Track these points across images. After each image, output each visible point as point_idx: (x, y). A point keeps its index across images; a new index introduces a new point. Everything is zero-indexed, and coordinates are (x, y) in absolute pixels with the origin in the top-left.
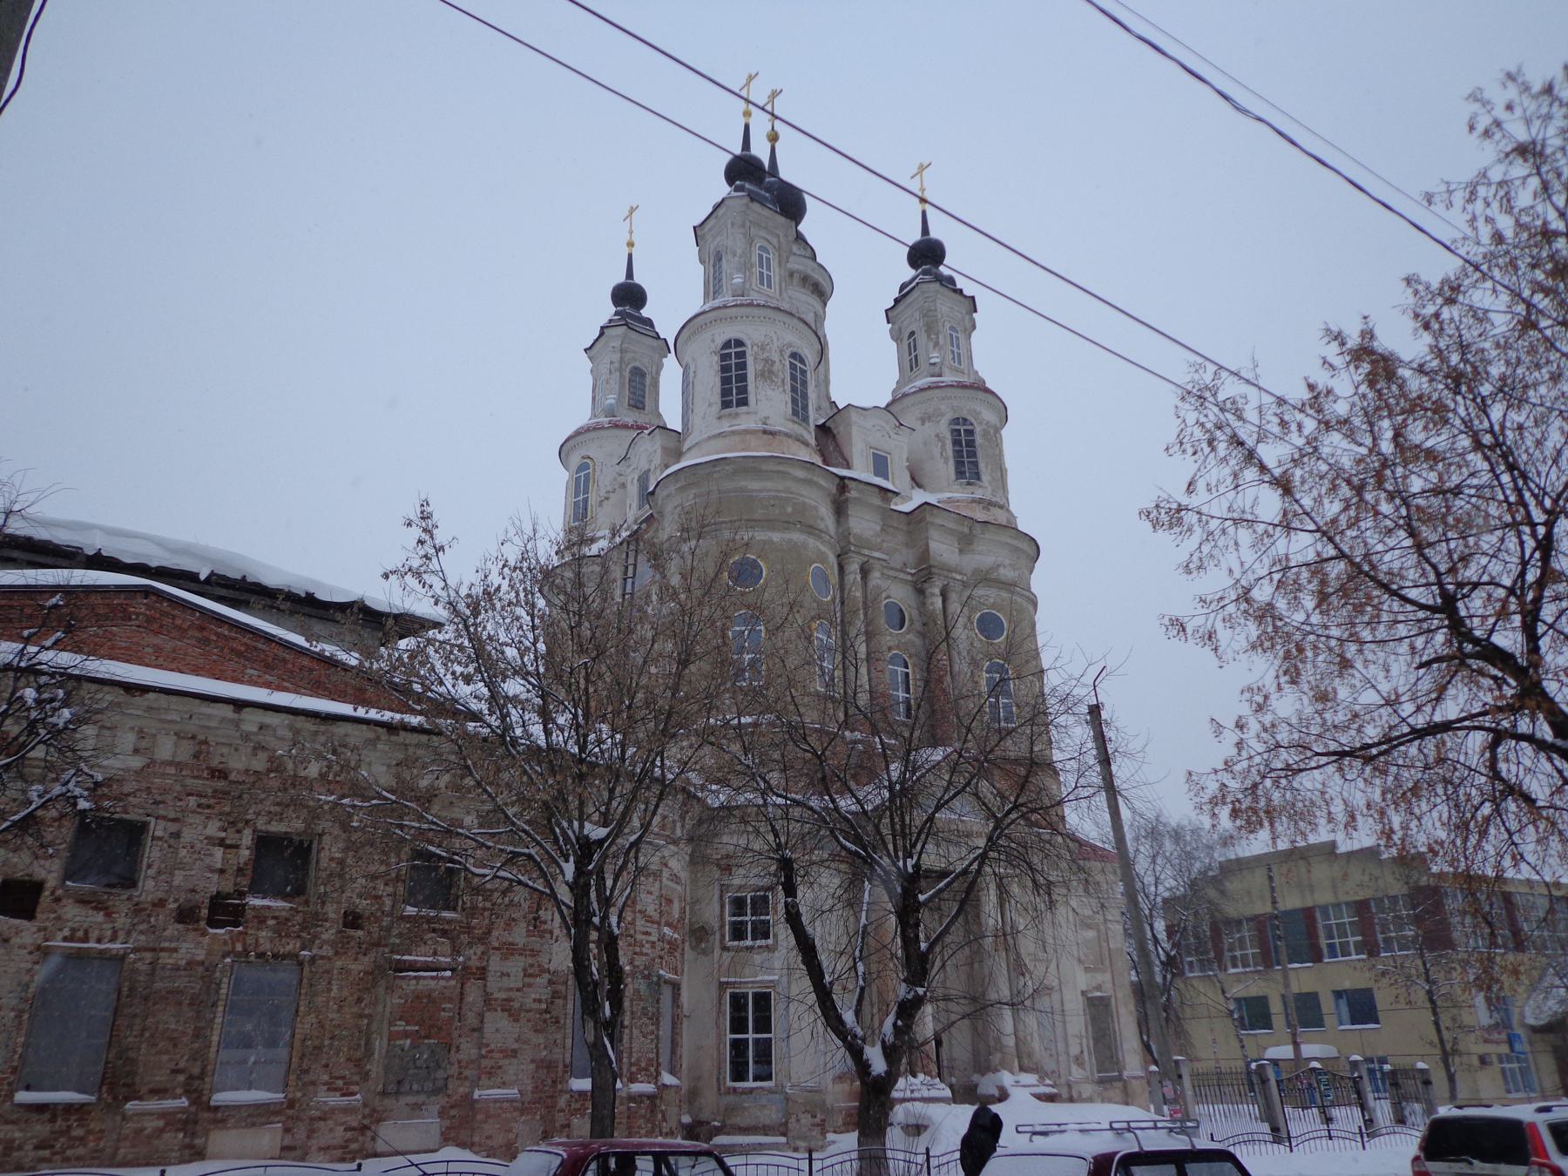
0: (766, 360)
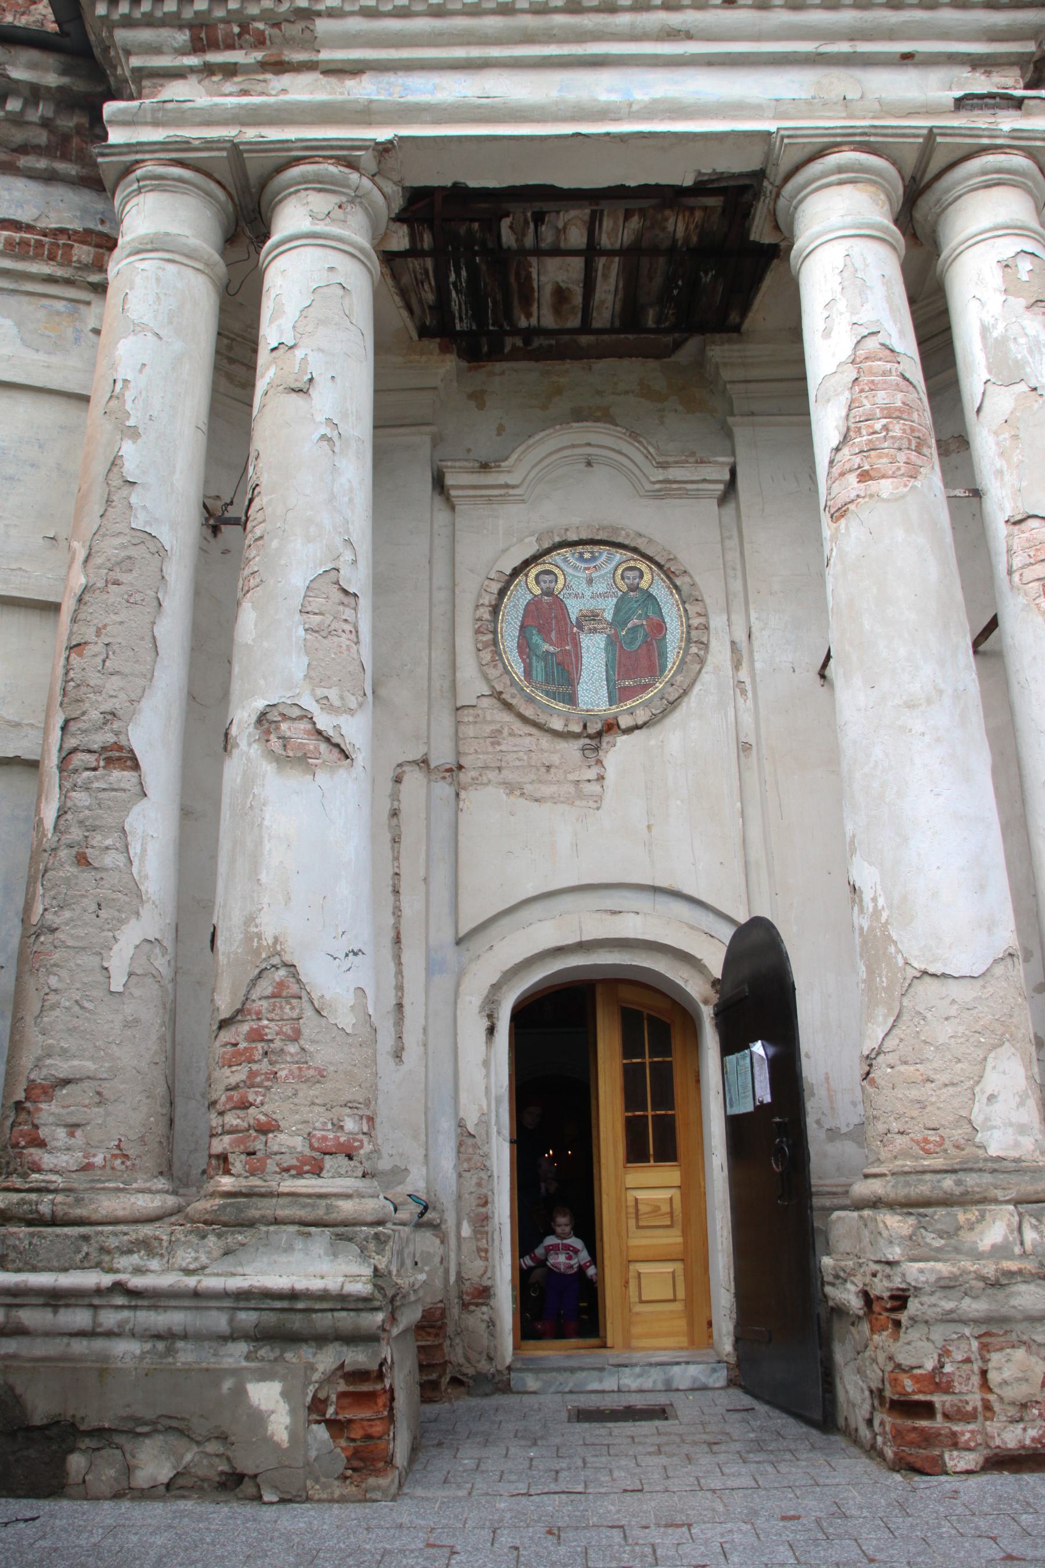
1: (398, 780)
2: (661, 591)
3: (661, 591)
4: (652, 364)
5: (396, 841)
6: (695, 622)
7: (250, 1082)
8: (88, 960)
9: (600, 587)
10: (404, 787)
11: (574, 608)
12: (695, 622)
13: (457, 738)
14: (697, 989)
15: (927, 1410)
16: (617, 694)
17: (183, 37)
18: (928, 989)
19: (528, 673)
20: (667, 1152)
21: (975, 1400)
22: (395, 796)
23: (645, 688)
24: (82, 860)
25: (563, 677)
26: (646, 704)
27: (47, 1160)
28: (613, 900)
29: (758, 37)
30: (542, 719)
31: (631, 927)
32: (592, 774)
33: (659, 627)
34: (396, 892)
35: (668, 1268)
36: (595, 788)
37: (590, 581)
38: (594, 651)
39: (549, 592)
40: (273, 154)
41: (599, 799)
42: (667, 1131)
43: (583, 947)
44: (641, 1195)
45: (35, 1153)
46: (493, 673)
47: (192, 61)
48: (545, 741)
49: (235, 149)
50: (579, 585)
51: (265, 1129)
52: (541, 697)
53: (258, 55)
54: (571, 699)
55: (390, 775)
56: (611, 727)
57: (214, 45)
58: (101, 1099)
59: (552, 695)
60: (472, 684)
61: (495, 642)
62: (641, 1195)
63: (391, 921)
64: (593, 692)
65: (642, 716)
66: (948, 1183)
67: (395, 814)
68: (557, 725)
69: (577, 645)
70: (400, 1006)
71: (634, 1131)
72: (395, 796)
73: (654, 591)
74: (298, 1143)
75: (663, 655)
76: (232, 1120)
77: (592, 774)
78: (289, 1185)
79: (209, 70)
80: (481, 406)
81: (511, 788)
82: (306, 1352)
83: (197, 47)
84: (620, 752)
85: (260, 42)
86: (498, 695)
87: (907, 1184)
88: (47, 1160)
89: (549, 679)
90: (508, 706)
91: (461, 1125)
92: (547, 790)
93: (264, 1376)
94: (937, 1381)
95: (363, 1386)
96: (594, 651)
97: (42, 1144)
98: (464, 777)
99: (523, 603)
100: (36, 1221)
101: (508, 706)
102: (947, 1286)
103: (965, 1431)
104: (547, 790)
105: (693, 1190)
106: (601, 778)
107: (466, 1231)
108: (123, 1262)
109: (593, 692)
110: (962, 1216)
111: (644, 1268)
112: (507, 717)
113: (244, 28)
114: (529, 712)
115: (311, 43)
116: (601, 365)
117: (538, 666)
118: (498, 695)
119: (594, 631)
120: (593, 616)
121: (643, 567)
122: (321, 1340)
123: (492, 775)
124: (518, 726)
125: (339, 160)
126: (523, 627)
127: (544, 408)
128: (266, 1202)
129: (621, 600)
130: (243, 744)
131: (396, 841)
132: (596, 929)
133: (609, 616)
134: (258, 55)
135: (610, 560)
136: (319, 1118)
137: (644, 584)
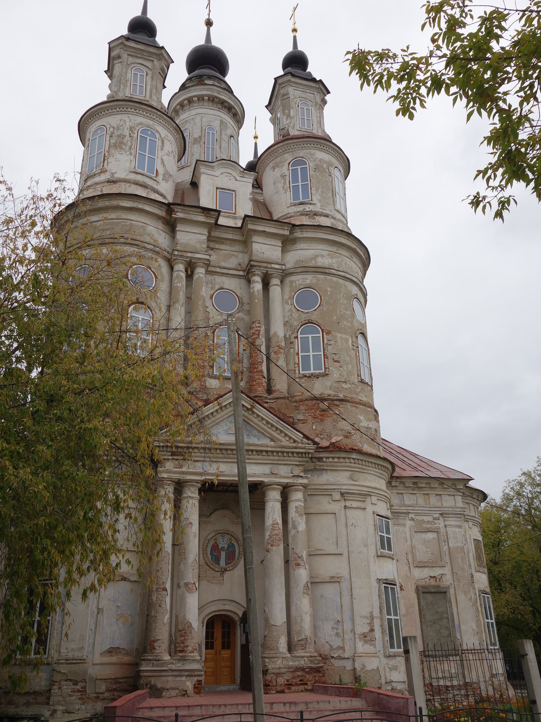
0: (119, 136)
2: (235, 544)
3: (235, 544)
7: (185, 639)
8: (161, 621)
9: (225, 542)
11: (220, 546)
14: (237, 618)
15: (269, 685)
16: (227, 564)
17: (170, 454)
18: (274, 627)
19: (212, 559)
20: (229, 648)
21: (275, 684)
23: (232, 563)
24: (160, 606)
25: (217, 560)
26: (232, 566)
27: (156, 652)
28: (225, 602)
30: (214, 568)
31: (227, 607)
32: (222, 579)
33: (235, 551)
35: (228, 669)
38: (223, 554)
39: (216, 543)
42: (229, 643)
43: (219, 611)
44: (224, 655)
45: (154, 651)
47: (171, 457)
48: (214, 572)
51: (187, 647)
52: (213, 563)
53: (182, 457)
54: (219, 564)
56: (226, 570)
57: (175, 455)
58: (163, 643)
62: (224, 655)
64: (223, 563)
65: (231, 568)
66: (274, 655)
68: (217, 570)
69: (220, 554)
71: (223, 643)
74: (191, 648)
75: (235, 557)
76: (181, 645)
77: (222, 579)
78: (190, 654)
79: (173, 459)
81: (208, 581)
82: (193, 678)
83: (172, 455)
84: (227, 575)
85: (182, 455)
86: (206, 563)
87: (57, 633)
88: (156, 652)
89: (215, 560)
90: (208, 565)
92: (214, 582)
93: (188, 681)
94: (270, 682)
95: (199, 682)
96: (223, 554)
97: (155, 649)
100: (157, 660)
101: (208, 565)
102: (273, 669)
103: (274, 688)
105: (233, 655)
108: (169, 666)
109: (223, 563)
110: (275, 660)
111: (224, 669)
112: (208, 567)
113: (180, 453)
114: (212, 567)
115: (190, 456)
117: (214, 557)
118: (206, 563)
120: (223, 548)
122: (195, 676)
123: (205, 578)
124: (210, 569)
125: (196, 482)
130: (182, 587)
132: (221, 608)
133: (226, 548)
134: (182, 457)
135: (227, 537)
136: (193, 645)
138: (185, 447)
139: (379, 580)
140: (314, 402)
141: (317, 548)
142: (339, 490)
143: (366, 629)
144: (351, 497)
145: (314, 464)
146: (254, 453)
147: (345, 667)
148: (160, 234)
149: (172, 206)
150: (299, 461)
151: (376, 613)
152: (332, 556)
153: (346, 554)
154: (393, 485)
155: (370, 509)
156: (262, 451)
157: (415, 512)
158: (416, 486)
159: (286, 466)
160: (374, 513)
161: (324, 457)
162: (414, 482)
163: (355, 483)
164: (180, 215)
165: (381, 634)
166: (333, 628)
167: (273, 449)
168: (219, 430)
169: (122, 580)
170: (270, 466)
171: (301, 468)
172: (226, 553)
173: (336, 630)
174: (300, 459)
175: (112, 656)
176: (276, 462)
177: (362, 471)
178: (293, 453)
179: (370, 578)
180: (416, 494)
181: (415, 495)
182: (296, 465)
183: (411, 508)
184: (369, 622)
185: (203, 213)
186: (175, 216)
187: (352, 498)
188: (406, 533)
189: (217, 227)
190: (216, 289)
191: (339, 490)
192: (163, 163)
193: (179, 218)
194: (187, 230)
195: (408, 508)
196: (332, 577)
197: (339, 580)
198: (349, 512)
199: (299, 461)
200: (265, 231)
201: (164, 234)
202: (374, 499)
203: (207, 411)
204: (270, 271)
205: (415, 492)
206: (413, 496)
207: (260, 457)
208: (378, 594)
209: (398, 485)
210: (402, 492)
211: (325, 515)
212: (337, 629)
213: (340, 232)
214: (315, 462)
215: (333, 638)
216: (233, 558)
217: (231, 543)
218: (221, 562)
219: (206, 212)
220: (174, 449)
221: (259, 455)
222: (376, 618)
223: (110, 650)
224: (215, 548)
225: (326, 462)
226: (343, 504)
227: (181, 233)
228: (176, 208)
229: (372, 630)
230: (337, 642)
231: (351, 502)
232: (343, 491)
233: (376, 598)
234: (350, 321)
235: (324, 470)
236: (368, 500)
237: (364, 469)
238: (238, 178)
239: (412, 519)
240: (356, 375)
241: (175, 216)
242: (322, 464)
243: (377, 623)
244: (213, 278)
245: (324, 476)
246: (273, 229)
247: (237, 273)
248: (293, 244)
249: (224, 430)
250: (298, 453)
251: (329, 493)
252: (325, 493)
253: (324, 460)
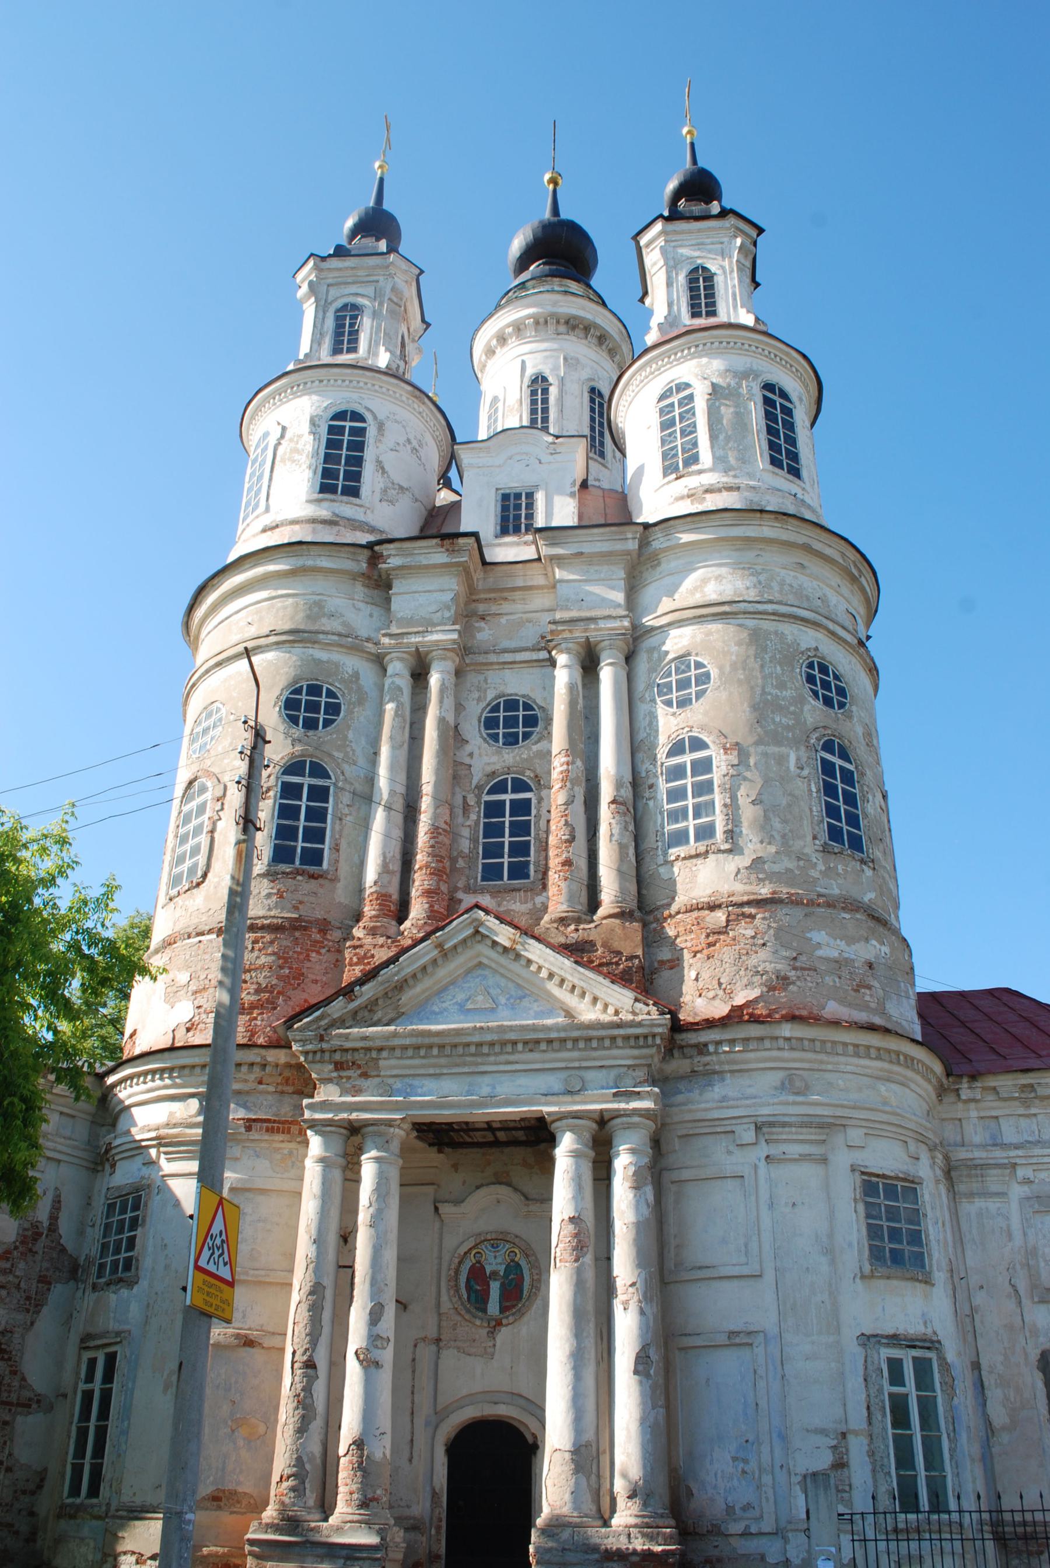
1: (415, 1346)
2: (523, 1263)
4: (529, 1149)
5: (414, 1372)
6: (535, 1277)
9: (499, 1260)
10: (418, 1349)
12: (535, 1277)
13: (439, 1327)
16: (503, 1309)
22: (414, 1353)
23: (514, 1306)
25: (480, 1300)
29: (544, 1062)
32: (491, 1344)
34: (413, 1393)
36: (490, 1350)
37: (495, 1257)
38: (495, 1287)
39: (479, 1262)
40: (422, 837)
41: (493, 1355)
46: (455, 1300)
49: (350, 1121)
50: (492, 1260)
54: (484, 1310)
55: (413, 1344)
57: (342, 1069)
59: (477, 1309)
60: (446, 1305)
61: (456, 1286)
63: (410, 1405)
64: (493, 1307)
67: (414, 1360)
69: (489, 1286)
70: (412, 1440)
72: (414, 1353)
73: (520, 1263)
80: (456, 1171)
81: (458, 1348)
84: (504, 1334)
89: (477, 1301)
91: (433, 1490)
92: (473, 1350)
96: (495, 1287)
98: (442, 1344)
99: (468, 1267)
104: (473, 1350)
106: (494, 1345)
107: (433, 1532)
109: (493, 1307)
112: (459, 1318)
115: (378, 1068)
116: (507, 1150)
117: (473, 1295)
119: (495, 1280)
120: (494, 1273)
121: (517, 1251)
126: (468, 1279)
127: (483, 1172)
128: (705, 1271)
129: (508, 1266)
131: (414, 1372)
133: (502, 1273)
137: (516, 1259)
138: (362, 1048)
139: (867, 1340)
140: (695, 914)
141: (698, 1265)
142: (753, 1119)
143: (823, 1461)
144: (782, 1133)
145: (688, 1061)
146: (520, 1047)
147: (763, 1557)
148: (359, 610)
149: (377, 548)
150: (635, 1058)
151: (857, 1419)
152: (736, 1283)
153: (769, 1276)
154: (963, 1097)
155: (842, 1159)
156: (537, 1042)
157: (1034, 1160)
158: (1033, 1095)
159: (604, 1071)
160: (853, 1170)
161: (712, 1042)
162: (1024, 1086)
163: (800, 1099)
164: (394, 562)
165: (870, 1474)
166: (735, 1459)
167: (563, 1035)
168: (444, 1005)
169: (245, 1344)
170: (563, 1075)
171: (641, 1074)
172: (502, 1285)
173: (741, 1465)
174: (636, 1052)
175: (219, 1508)
176: (576, 1064)
177: (816, 1066)
178: (613, 1039)
179: (838, 1330)
180: (1035, 1115)
181: (1034, 1120)
182: (629, 1067)
183: (1020, 1153)
184: (834, 1443)
185: (442, 546)
186: (386, 566)
187: (784, 1137)
188: (1008, 1219)
189: (489, 567)
190: (489, 699)
191: (753, 1119)
192: (383, 468)
193: (394, 569)
194: (414, 588)
195: (1013, 1153)
196: (732, 1334)
197: (750, 1341)
198: (781, 1172)
199: (635, 1058)
200: (582, 553)
201: (367, 609)
202: (855, 1135)
203: (408, 966)
204: (594, 636)
205: (1033, 1111)
206: (1028, 1121)
207: (536, 1056)
208: (861, 1372)
209: (979, 1097)
210: (994, 1113)
211: (719, 1182)
212: (746, 1461)
213: (758, 515)
214: (691, 1057)
215: (735, 1482)
216: (519, 1297)
217: (513, 1261)
218: (489, 1305)
219: (447, 542)
220: (337, 1057)
221: (531, 1051)
222: (856, 1433)
223: (216, 1494)
224: (478, 1276)
225: (716, 1053)
226: (763, 1150)
227: (399, 597)
228: (385, 549)
229: (840, 1465)
230: (744, 1494)
231: (783, 1147)
232: (760, 1119)
233: (855, 1384)
234: (792, 713)
235: (715, 1072)
236: (839, 1139)
237: (822, 1062)
238: (546, 458)
239: (1027, 1181)
240: (809, 838)
241: (386, 566)
242: (708, 1059)
243: (857, 1450)
244: (481, 678)
245: (716, 1089)
246: (599, 544)
247: (535, 656)
248: (654, 567)
249: (456, 1003)
250: (626, 1038)
251: (729, 1129)
252: (719, 1130)
253: (711, 1048)
